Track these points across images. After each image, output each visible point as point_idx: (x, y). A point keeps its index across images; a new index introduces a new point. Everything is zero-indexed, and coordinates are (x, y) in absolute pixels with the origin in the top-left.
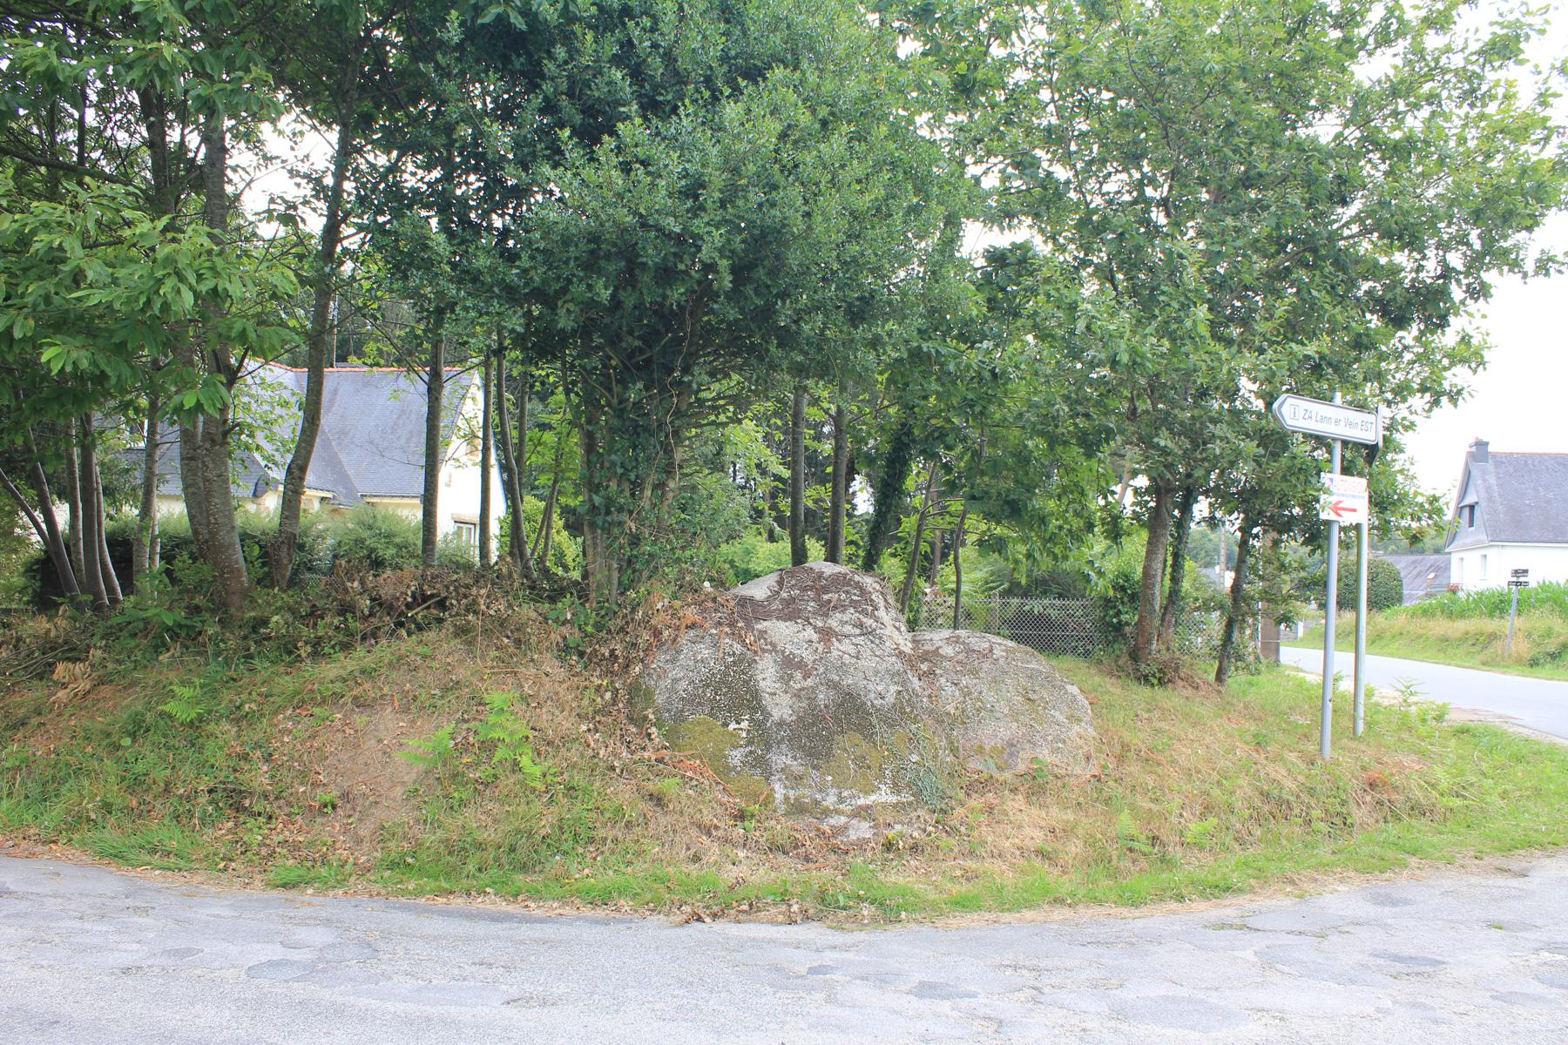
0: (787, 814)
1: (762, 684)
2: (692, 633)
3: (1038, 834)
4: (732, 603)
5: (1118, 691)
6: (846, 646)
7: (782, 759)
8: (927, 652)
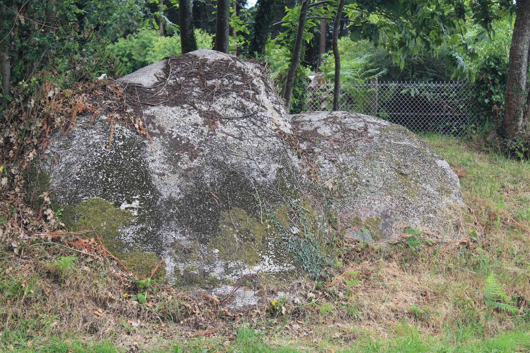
0: (178, 285)
1: (151, 165)
2: (83, 120)
3: (411, 298)
4: (121, 91)
5: (485, 164)
6: (230, 129)
7: (172, 235)
8: (306, 133)
